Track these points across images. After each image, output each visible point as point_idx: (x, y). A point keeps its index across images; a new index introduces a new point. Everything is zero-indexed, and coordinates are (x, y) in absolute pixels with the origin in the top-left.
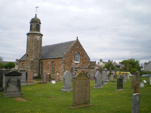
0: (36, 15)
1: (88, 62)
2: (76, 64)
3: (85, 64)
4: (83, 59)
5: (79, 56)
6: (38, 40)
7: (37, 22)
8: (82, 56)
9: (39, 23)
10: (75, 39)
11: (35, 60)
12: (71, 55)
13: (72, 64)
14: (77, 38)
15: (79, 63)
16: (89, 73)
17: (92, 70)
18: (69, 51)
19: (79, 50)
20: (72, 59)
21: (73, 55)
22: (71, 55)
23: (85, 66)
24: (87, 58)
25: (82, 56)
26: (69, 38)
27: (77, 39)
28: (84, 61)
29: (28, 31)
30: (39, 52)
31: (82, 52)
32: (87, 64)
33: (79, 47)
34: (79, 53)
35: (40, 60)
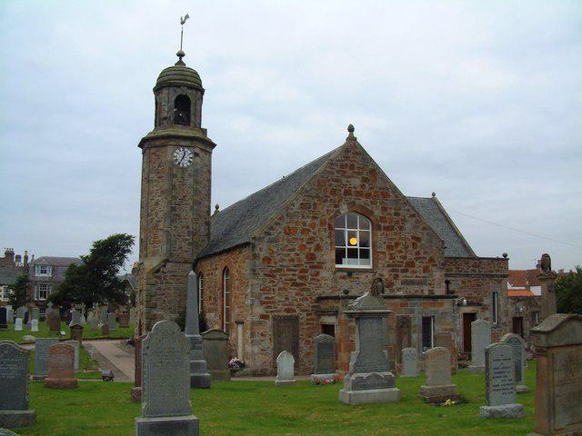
0: (181, 55)
1: (431, 260)
2: (344, 278)
3: (406, 271)
4: (397, 244)
5: (370, 230)
6: (183, 168)
7: (179, 86)
8: (386, 229)
9: (191, 87)
10: (340, 139)
11: (169, 266)
12: (313, 226)
13: (317, 274)
14: (351, 129)
15: (370, 267)
16: (237, 357)
17: (442, 304)
18: (297, 205)
19: (368, 195)
20: (318, 248)
21: (323, 223)
22: (313, 226)
23: (412, 283)
24: (418, 239)
25: (386, 229)
26: (323, 141)
27: (352, 139)
28: (405, 258)
29: (147, 126)
30: (190, 225)
31: (384, 209)
32: (426, 269)
33: (365, 180)
34: (366, 214)
35: (198, 260)
